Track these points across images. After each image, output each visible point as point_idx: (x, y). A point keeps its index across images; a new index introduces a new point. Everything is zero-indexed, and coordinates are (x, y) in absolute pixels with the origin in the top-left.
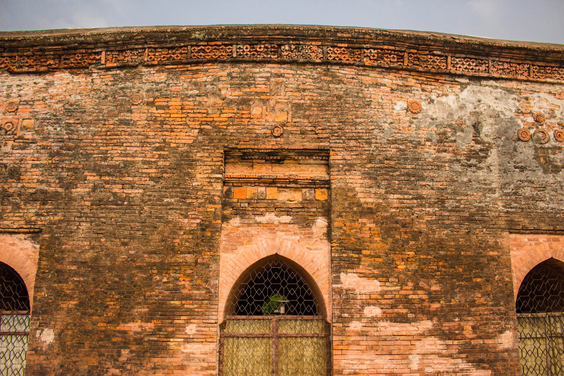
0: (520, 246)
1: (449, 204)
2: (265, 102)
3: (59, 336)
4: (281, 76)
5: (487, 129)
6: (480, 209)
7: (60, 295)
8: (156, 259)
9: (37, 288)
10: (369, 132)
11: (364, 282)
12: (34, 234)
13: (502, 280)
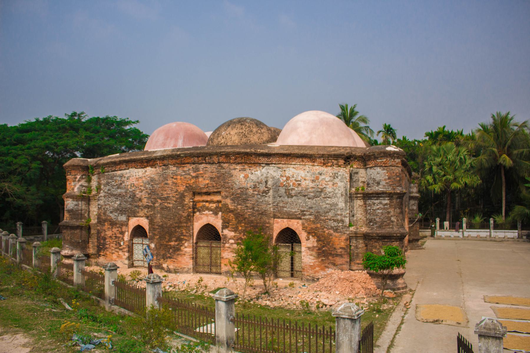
0: (278, 223)
1: (256, 209)
2: (202, 177)
3: (155, 245)
4: (206, 168)
5: (270, 183)
6: (265, 210)
7: (155, 235)
8: (177, 225)
9: (149, 233)
10: (232, 185)
11: (230, 232)
12: (147, 217)
13: (269, 234)
